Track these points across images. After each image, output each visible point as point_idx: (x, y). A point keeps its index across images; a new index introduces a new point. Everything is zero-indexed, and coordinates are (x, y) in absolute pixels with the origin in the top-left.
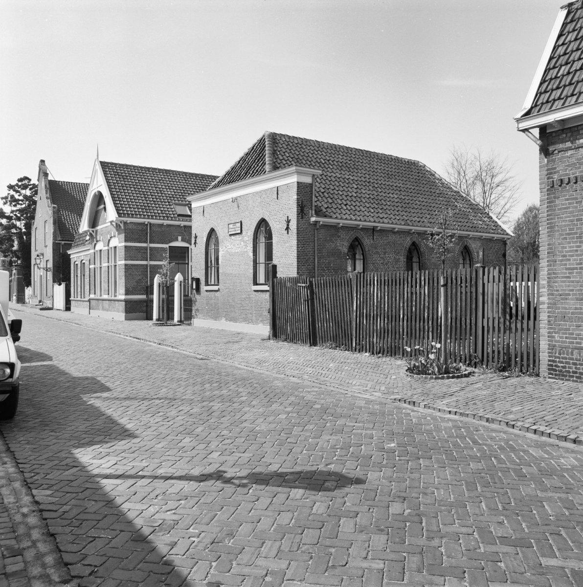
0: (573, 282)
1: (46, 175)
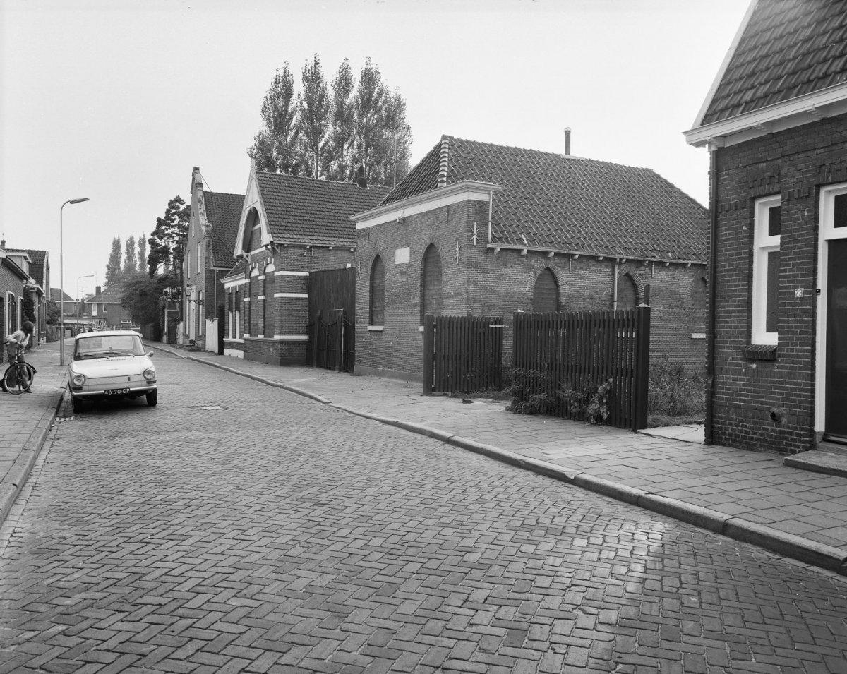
0: (730, 327)
1: (201, 185)
